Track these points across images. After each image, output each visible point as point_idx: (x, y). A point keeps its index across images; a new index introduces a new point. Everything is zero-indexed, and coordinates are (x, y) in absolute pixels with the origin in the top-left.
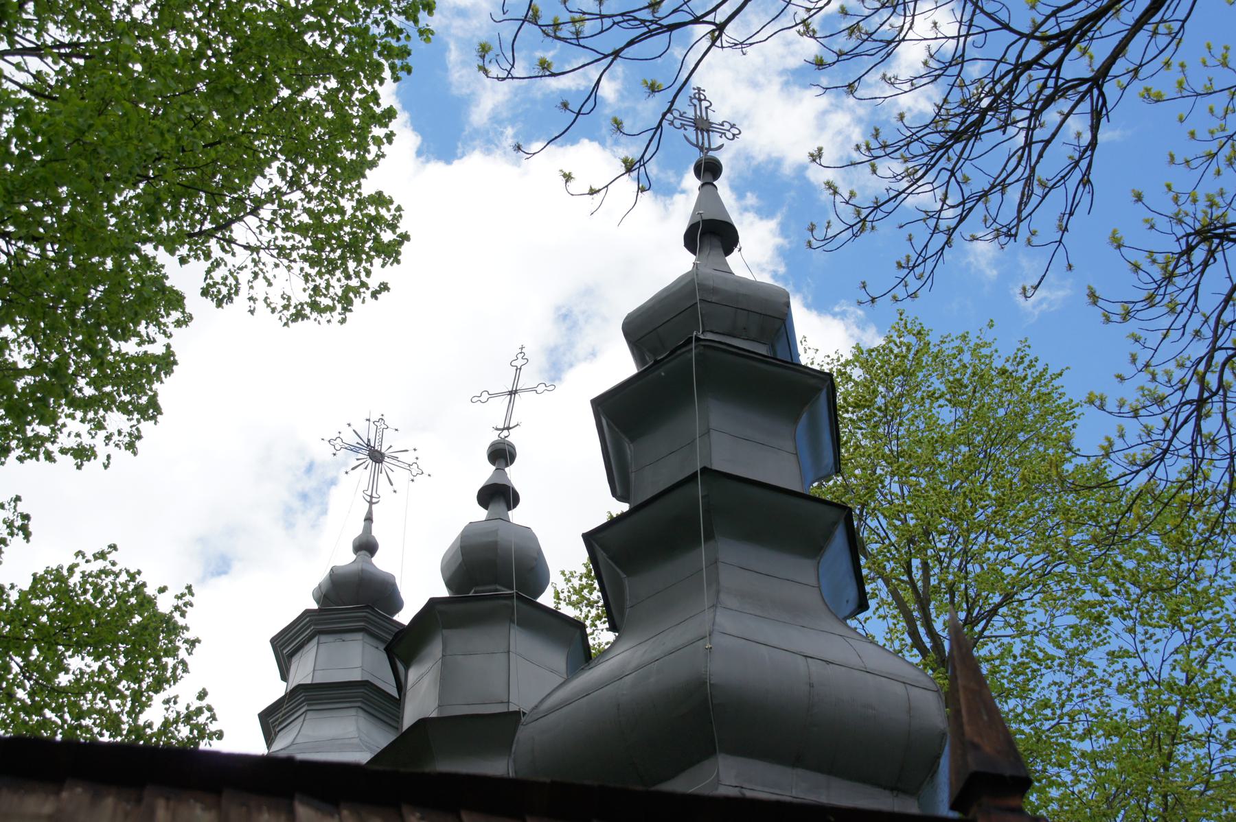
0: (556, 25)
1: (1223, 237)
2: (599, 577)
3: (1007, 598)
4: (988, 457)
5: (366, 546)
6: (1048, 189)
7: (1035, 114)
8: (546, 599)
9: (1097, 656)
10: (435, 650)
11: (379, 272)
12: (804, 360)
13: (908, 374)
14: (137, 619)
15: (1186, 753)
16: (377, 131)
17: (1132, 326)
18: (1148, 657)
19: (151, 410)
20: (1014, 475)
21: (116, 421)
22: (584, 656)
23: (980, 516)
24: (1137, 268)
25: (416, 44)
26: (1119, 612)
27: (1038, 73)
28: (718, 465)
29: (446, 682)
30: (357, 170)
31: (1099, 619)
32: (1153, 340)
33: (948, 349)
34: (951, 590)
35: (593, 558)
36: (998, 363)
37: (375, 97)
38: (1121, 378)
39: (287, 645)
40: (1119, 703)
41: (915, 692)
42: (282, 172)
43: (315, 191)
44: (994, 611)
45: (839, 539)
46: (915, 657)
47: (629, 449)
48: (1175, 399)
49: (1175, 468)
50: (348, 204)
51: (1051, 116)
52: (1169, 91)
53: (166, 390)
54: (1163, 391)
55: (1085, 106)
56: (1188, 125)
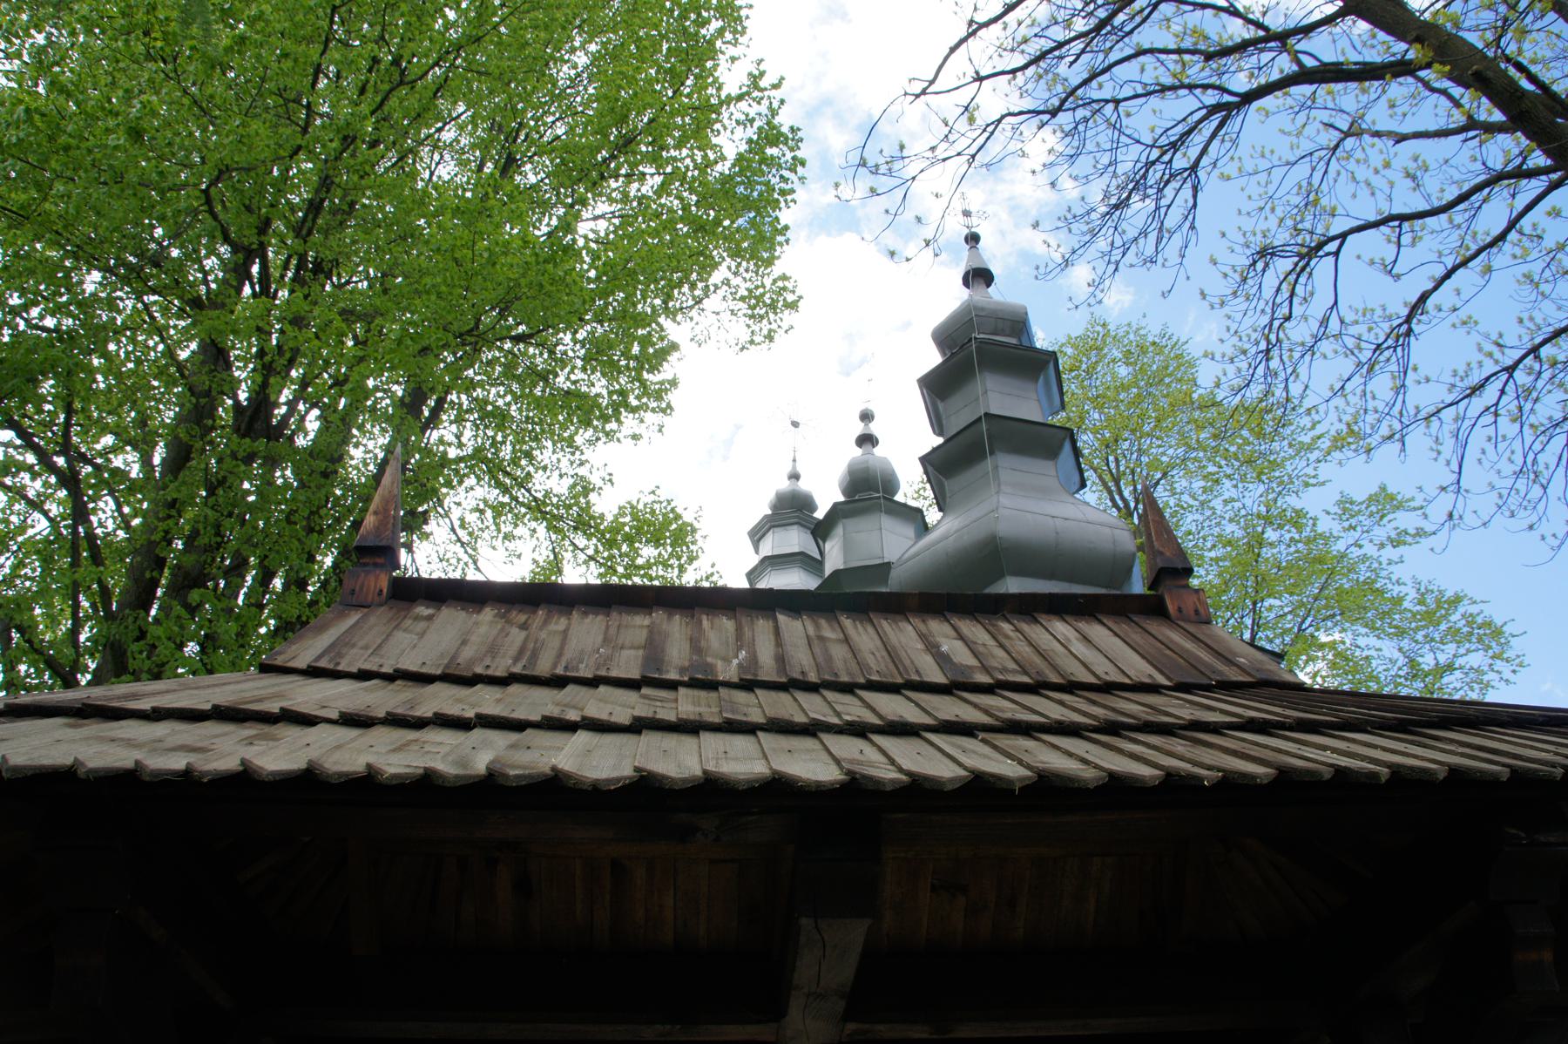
0: (877, 166)
1: (1273, 254)
2: (929, 481)
3: (1165, 475)
4: (1149, 394)
5: (795, 476)
6: (1171, 233)
7: (1160, 190)
8: (899, 498)
9: (1217, 504)
10: (839, 531)
11: (787, 317)
12: (1038, 345)
13: (1099, 349)
14: (674, 526)
15: (1266, 552)
16: (780, 238)
17: (1226, 310)
18: (1245, 501)
19: (667, 410)
20: (1164, 403)
21: (649, 417)
22: (924, 528)
23: (1147, 428)
24: (1226, 275)
25: (797, 185)
26: (1228, 477)
27: (1159, 167)
28: (994, 411)
29: (847, 548)
30: (769, 262)
31: (1217, 482)
32: (1238, 316)
33: (1121, 333)
34: (1133, 473)
35: (926, 472)
36: (1150, 339)
37: (777, 219)
38: (1222, 341)
39: (757, 535)
40: (1230, 528)
41: (1117, 532)
42: (729, 268)
43: (748, 276)
44: (1157, 483)
45: (1067, 446)
46: (1114, 512)
47: (941, 406)
48: (1253, 350)
49: (1255, 391)
50: (768, 282)
51: (1169, 192)
52: (1234, 174)
53: (672, 397)
54: (1247, 346)
55: (1188, 185)
56: (1247, 193)
